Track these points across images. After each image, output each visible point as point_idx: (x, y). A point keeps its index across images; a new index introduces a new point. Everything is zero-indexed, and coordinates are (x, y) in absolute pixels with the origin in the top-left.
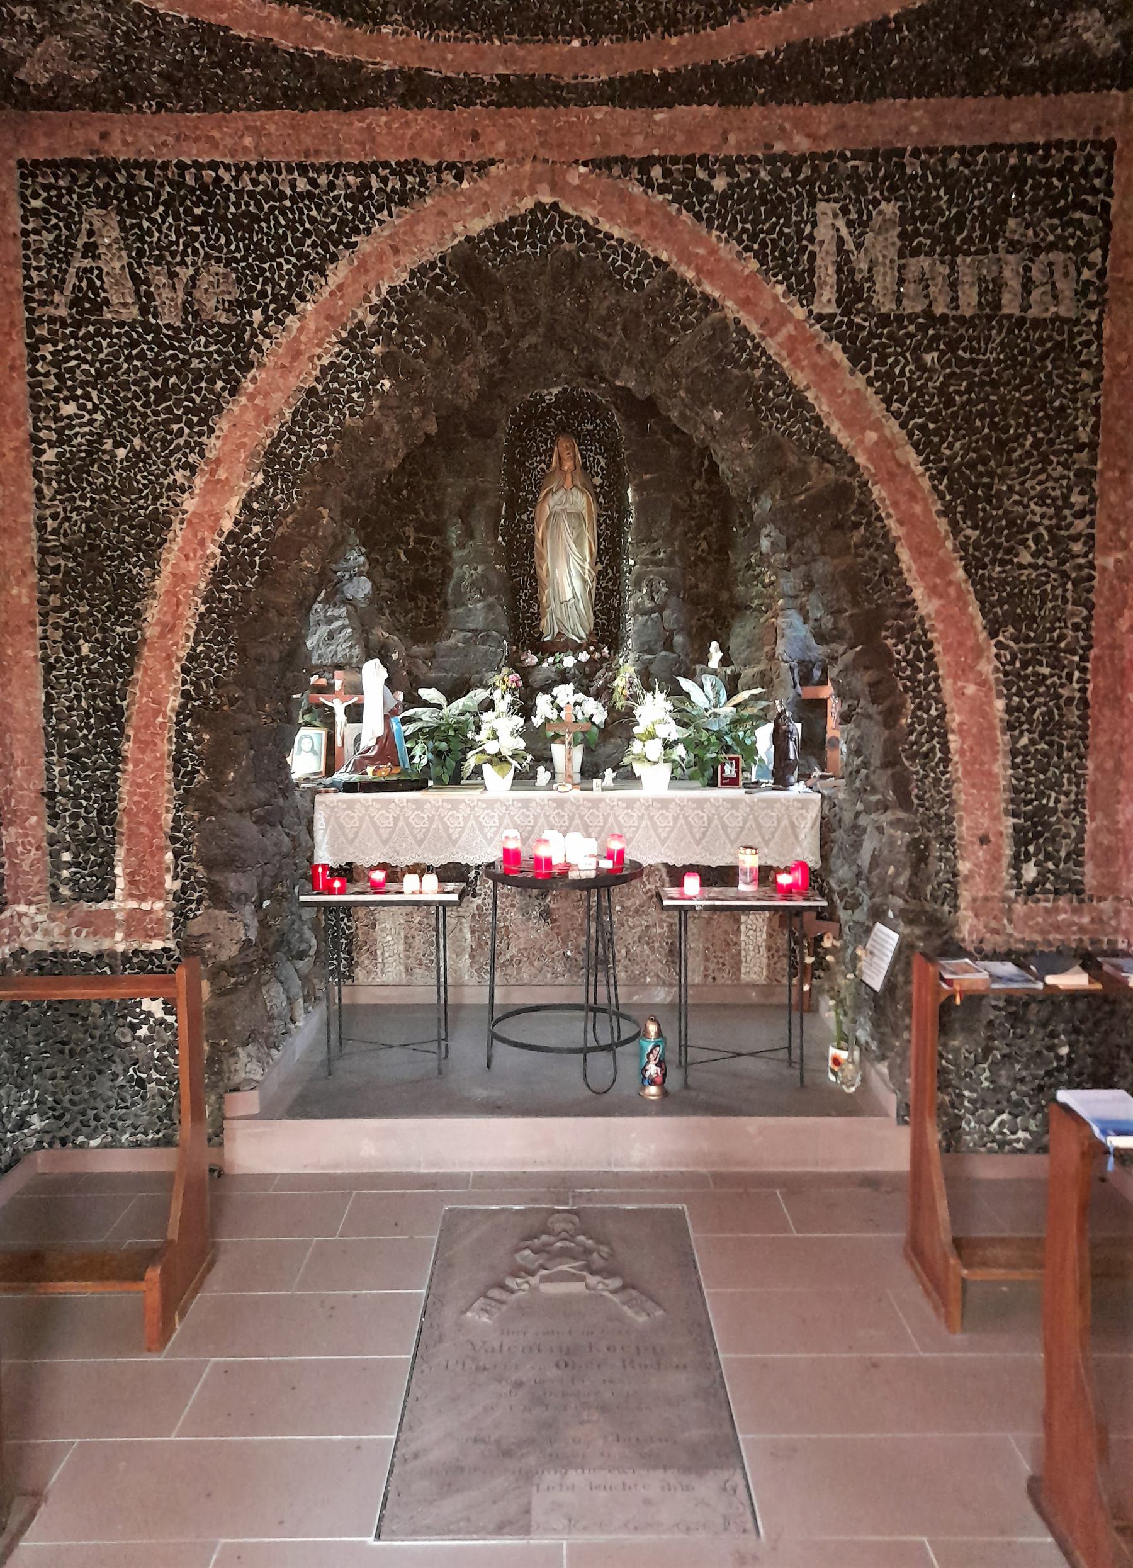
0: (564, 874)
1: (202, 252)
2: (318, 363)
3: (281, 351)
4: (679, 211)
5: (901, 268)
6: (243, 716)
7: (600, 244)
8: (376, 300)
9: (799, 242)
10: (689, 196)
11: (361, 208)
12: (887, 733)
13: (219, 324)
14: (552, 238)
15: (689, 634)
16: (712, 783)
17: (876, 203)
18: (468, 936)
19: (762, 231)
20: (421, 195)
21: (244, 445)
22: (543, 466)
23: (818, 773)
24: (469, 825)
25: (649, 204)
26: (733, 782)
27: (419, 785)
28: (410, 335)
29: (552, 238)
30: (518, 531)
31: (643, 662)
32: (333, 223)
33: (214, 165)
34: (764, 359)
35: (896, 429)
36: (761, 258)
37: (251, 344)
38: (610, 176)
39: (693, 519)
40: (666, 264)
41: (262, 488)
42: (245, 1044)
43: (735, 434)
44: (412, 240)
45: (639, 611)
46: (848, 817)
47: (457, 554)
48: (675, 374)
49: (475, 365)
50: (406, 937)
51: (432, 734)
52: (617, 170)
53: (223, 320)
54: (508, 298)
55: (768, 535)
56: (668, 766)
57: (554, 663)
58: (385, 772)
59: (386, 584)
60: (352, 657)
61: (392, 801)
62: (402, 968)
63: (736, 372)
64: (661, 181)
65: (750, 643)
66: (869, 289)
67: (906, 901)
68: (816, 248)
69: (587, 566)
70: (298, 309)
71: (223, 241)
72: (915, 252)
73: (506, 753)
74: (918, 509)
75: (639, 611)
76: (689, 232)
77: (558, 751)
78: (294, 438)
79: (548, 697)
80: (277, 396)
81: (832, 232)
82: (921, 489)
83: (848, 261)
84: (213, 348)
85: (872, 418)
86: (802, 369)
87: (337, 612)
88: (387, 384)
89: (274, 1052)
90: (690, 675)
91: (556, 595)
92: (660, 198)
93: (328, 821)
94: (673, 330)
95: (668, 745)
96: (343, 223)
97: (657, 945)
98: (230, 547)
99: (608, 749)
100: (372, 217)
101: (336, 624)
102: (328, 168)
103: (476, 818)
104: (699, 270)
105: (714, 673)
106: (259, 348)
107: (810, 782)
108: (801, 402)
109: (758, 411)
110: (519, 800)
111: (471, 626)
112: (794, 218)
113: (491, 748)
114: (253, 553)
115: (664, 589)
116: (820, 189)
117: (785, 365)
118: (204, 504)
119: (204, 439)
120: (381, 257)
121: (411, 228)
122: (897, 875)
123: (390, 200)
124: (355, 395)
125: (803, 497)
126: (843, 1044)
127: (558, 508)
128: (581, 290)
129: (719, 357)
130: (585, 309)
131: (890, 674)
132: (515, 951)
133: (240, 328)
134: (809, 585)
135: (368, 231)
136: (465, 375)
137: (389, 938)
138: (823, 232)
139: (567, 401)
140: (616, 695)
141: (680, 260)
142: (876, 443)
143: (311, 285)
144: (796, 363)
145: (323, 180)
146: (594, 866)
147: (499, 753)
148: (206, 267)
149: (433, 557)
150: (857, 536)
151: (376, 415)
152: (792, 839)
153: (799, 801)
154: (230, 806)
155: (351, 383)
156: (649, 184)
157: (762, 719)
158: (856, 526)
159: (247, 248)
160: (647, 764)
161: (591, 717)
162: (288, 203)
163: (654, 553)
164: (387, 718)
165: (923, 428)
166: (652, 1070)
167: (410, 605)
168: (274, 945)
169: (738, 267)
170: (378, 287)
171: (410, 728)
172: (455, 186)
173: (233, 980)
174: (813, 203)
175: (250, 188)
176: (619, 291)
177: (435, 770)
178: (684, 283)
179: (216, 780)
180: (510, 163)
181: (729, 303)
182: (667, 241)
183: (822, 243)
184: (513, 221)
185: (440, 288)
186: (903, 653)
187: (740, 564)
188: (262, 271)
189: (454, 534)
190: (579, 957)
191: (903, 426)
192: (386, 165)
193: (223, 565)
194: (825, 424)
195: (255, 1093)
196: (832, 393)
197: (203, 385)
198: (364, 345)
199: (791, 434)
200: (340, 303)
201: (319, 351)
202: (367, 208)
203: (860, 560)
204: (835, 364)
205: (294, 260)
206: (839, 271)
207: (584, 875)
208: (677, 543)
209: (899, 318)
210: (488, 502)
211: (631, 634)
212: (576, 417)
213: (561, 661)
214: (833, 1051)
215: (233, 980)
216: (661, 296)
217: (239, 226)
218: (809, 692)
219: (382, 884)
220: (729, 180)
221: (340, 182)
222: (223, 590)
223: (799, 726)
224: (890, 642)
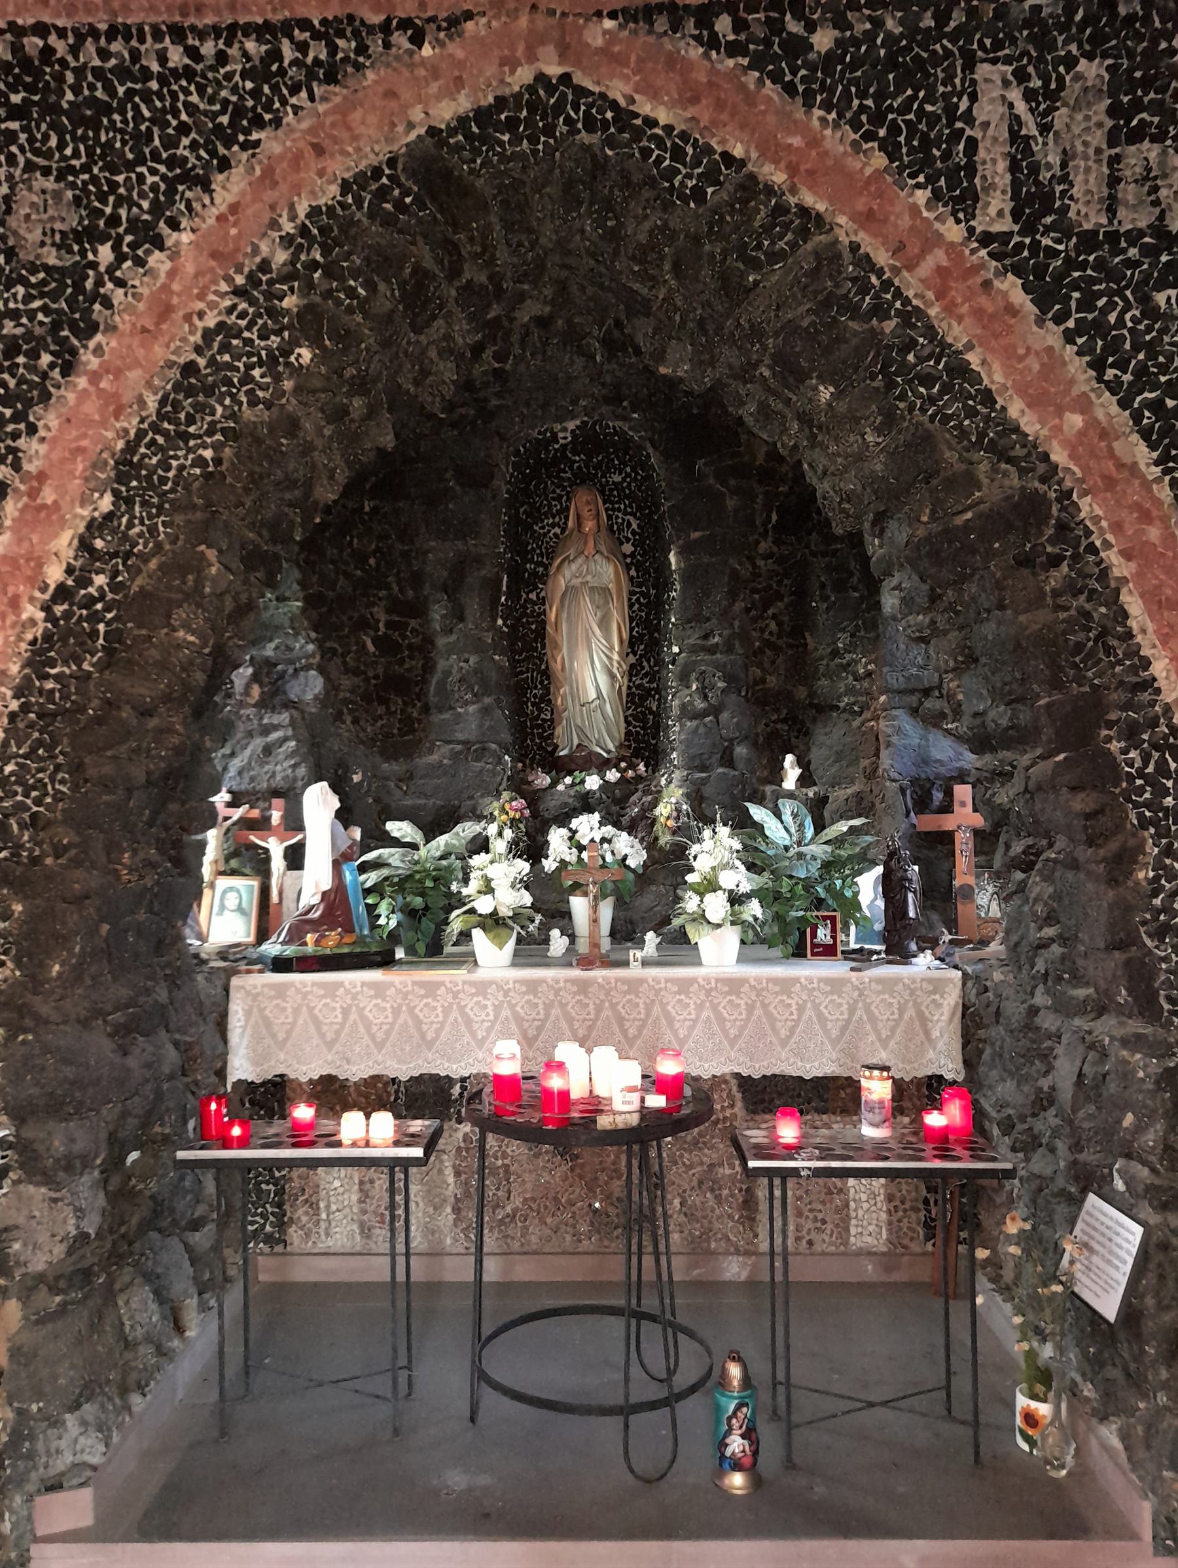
0: (589, 1122)
1: (21, 160)
2: (199, 324)
3: (141, 306)
4: (760, 81)
5: (1115, 160)
6: (79, 873)
7: (638, 134)
8: (288, 227)
9: (950, 124)
10: (776, 58)
11: (266, 89)
12: (1111, 893)
13: (47, 269)
14: (562, 128)
15: (755, 744)
16: (799, 953)
17: (1070, 62)
18: (451, 1180)
19: (890, 109)
20: (358, 67)
21: (81, 450)
22: (557, 530)
23: (947, 937)
24: (451, 1019)
25: (713, 71)
26: (829, 951)
27: (385, 961)
28: (342, 279)
29: (562, 128)
30: (525, 614)
31: (693, 783)
32: (223, 112)
33: (41, 29)
34: (898, 304)
35: (1115, 409)
36: (890, 149)
37: (95, 296)
38: (651, 32)
39: (757, 591)
40: (742, 163)
41: (109, 516)
42: (75, 1407)
43: (856, 420)
44: (345, 135)
45: (687, 712)
46: (1014, 1010)
47: (441, 642)
48: (756, 333)
49: (447, 337)
50: (361, 1183)
51: (402, 884)
52: (661, 23)
53: (52, 261)
54: (494, 219)
55: (898, 588)
56: (738, 928)
57: (573, 785)
58: (332, 941)
59: (346, 682)
60: (295, 779)
61: (340, 984)
62: (355, 1227)
63: (854, 325)
64: (731, 37)
65: (839, 757)
66: (1063, 193)
67: (1153, 1170)
68: (977, 133)
69: (616, 657)
70: (169, 243)
71: (53, 142)
72: (1135, 136)
73: (505, 912)
74: (1154, 533)
75: (687, 712)
76: (777, 113)
77: (579, 905)
78: (160, 440)
79: (564, 832)
80: (134, 375)
81: (1002, 109)
82: (1159, 503)
83: (1028, 152)
84: (36, 304)
85: (1075, 391)
86: (960, 319)
87: (276, 719)
88: (305, 354)
89: (136, 1400)
90: (760, 801)
91: (575, 694)
92: (731, 63)
93: (248, 1014)
94: (755, 265)
95: (735, 899)
96: (238, 112)
97: (726, 1192)
98: (59, 610)
99: (647, 900)
100: (284, 102)
101: (275, 735)
102: (216, 31)
103: (462, 1009)
104: (792, 170)
105: (791, 795)
106: (107, 303)
107: (939, 951)
108: (961, 370)
109: (891, 385)
110: (522, 982)
111: (460, 736)
112: (941, 89)
113: (484, 905)
114: (95, 618)
115: (721, 684)
116: (980, 42)
117: (932, 312)
118: (19, 541)
119: (21, 443)
120: (296, 161)
121: (345, 115)
122: (1138, 1129)
123: (311, 75)
124: (256, 373)
125: (969, 515)
126: (1040, 1389)
127: (576, 582)
128: (608, 205)
129: (826, 304)
130: (614, 236)
131: (1115, 797)
132: (517, 1202)
133: (78, 273)
134: (968, 660)
135: (277, 122)
136: (433, 353)
137: (337, 1183)
138: (988, 110)
139: (587, 440)
140: (657, 828)
141: (762, 154)
142: (1082, 433)
143: (189, 207)
144: (950, 309)
145: (208, 49)
146: (636, 1105)
147: (495, 913)
148: (27, 183)
149: (410, 647)
150: (1057, 577)
151: (292, 405)
152: (922, 1036)
153: (930, 981)
154: (55, 1017)
155: (249, 355)
156: (713, 42)
157: (864, 862)
158: (1055, 561)
159: (90, 153)
160: (706, 928)
161: (625, 858)
162: (154, 85)
163: (706, 637)
164: (337, 865)
165: (1157, 406)
166: (736, 1445)
167: (381, 710)
168: (140, 1225)
169: (854, 163)
170: (292, 208)
171: (372, 878)
172: (411, 53)
173: (58, 1299)
174: (970, 64)
175: (97, 62)
176: (667, 206)
177: (407, 935)
178: (769, 190)
179: (32, 977)
180: (497, 16)
181: (842, 220)
182: (743, 127)
183: (986, 125)
184: (501, 102)
185: (388, 206)
186: (1138, 764)
187: (824, 650)
188: (113, 186)
189: (437, 613)
190: (612, 1211)
191: (1124, 404)
192: (305, 24)
193: (47, 637)
194: (1000, 402)
195: (87, 1494)
196: (1009, 355)
197: (21, 360)
198: (270, 295)
199: (946, 419)
200: (234, 231)
201: (200, 305)
202: (275, 88)
203: (1062, 615)
204: (1011, 310)
205: (162, 169)
206: (1014, 167)
207: (620, 1122)
208: (737, 623)
209: (1113, 237)
210: (483, 572)
211: (676, 744)
212: (598, 466)
213: (583, 782)
214: (1022, 1401)
215: (58, 1299)
216: (732, 212)
217: (79, 120)
218: (928, 822)
219: (310, 1126)
220: (837, 33)
221: (234, 51)
222: (47, 676)
223: (916, 868)
224: (1115, 746)
